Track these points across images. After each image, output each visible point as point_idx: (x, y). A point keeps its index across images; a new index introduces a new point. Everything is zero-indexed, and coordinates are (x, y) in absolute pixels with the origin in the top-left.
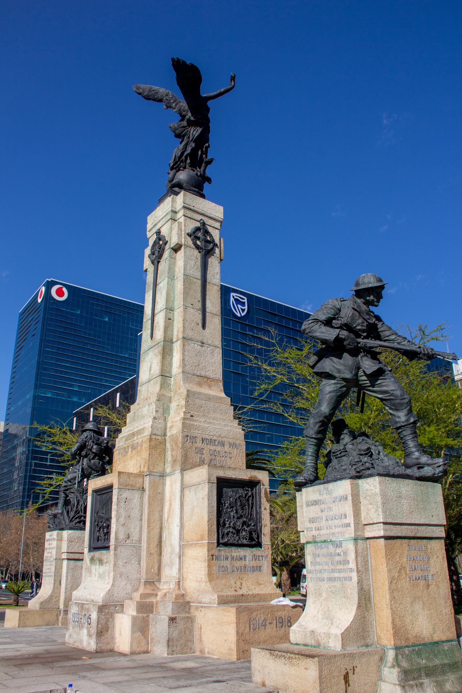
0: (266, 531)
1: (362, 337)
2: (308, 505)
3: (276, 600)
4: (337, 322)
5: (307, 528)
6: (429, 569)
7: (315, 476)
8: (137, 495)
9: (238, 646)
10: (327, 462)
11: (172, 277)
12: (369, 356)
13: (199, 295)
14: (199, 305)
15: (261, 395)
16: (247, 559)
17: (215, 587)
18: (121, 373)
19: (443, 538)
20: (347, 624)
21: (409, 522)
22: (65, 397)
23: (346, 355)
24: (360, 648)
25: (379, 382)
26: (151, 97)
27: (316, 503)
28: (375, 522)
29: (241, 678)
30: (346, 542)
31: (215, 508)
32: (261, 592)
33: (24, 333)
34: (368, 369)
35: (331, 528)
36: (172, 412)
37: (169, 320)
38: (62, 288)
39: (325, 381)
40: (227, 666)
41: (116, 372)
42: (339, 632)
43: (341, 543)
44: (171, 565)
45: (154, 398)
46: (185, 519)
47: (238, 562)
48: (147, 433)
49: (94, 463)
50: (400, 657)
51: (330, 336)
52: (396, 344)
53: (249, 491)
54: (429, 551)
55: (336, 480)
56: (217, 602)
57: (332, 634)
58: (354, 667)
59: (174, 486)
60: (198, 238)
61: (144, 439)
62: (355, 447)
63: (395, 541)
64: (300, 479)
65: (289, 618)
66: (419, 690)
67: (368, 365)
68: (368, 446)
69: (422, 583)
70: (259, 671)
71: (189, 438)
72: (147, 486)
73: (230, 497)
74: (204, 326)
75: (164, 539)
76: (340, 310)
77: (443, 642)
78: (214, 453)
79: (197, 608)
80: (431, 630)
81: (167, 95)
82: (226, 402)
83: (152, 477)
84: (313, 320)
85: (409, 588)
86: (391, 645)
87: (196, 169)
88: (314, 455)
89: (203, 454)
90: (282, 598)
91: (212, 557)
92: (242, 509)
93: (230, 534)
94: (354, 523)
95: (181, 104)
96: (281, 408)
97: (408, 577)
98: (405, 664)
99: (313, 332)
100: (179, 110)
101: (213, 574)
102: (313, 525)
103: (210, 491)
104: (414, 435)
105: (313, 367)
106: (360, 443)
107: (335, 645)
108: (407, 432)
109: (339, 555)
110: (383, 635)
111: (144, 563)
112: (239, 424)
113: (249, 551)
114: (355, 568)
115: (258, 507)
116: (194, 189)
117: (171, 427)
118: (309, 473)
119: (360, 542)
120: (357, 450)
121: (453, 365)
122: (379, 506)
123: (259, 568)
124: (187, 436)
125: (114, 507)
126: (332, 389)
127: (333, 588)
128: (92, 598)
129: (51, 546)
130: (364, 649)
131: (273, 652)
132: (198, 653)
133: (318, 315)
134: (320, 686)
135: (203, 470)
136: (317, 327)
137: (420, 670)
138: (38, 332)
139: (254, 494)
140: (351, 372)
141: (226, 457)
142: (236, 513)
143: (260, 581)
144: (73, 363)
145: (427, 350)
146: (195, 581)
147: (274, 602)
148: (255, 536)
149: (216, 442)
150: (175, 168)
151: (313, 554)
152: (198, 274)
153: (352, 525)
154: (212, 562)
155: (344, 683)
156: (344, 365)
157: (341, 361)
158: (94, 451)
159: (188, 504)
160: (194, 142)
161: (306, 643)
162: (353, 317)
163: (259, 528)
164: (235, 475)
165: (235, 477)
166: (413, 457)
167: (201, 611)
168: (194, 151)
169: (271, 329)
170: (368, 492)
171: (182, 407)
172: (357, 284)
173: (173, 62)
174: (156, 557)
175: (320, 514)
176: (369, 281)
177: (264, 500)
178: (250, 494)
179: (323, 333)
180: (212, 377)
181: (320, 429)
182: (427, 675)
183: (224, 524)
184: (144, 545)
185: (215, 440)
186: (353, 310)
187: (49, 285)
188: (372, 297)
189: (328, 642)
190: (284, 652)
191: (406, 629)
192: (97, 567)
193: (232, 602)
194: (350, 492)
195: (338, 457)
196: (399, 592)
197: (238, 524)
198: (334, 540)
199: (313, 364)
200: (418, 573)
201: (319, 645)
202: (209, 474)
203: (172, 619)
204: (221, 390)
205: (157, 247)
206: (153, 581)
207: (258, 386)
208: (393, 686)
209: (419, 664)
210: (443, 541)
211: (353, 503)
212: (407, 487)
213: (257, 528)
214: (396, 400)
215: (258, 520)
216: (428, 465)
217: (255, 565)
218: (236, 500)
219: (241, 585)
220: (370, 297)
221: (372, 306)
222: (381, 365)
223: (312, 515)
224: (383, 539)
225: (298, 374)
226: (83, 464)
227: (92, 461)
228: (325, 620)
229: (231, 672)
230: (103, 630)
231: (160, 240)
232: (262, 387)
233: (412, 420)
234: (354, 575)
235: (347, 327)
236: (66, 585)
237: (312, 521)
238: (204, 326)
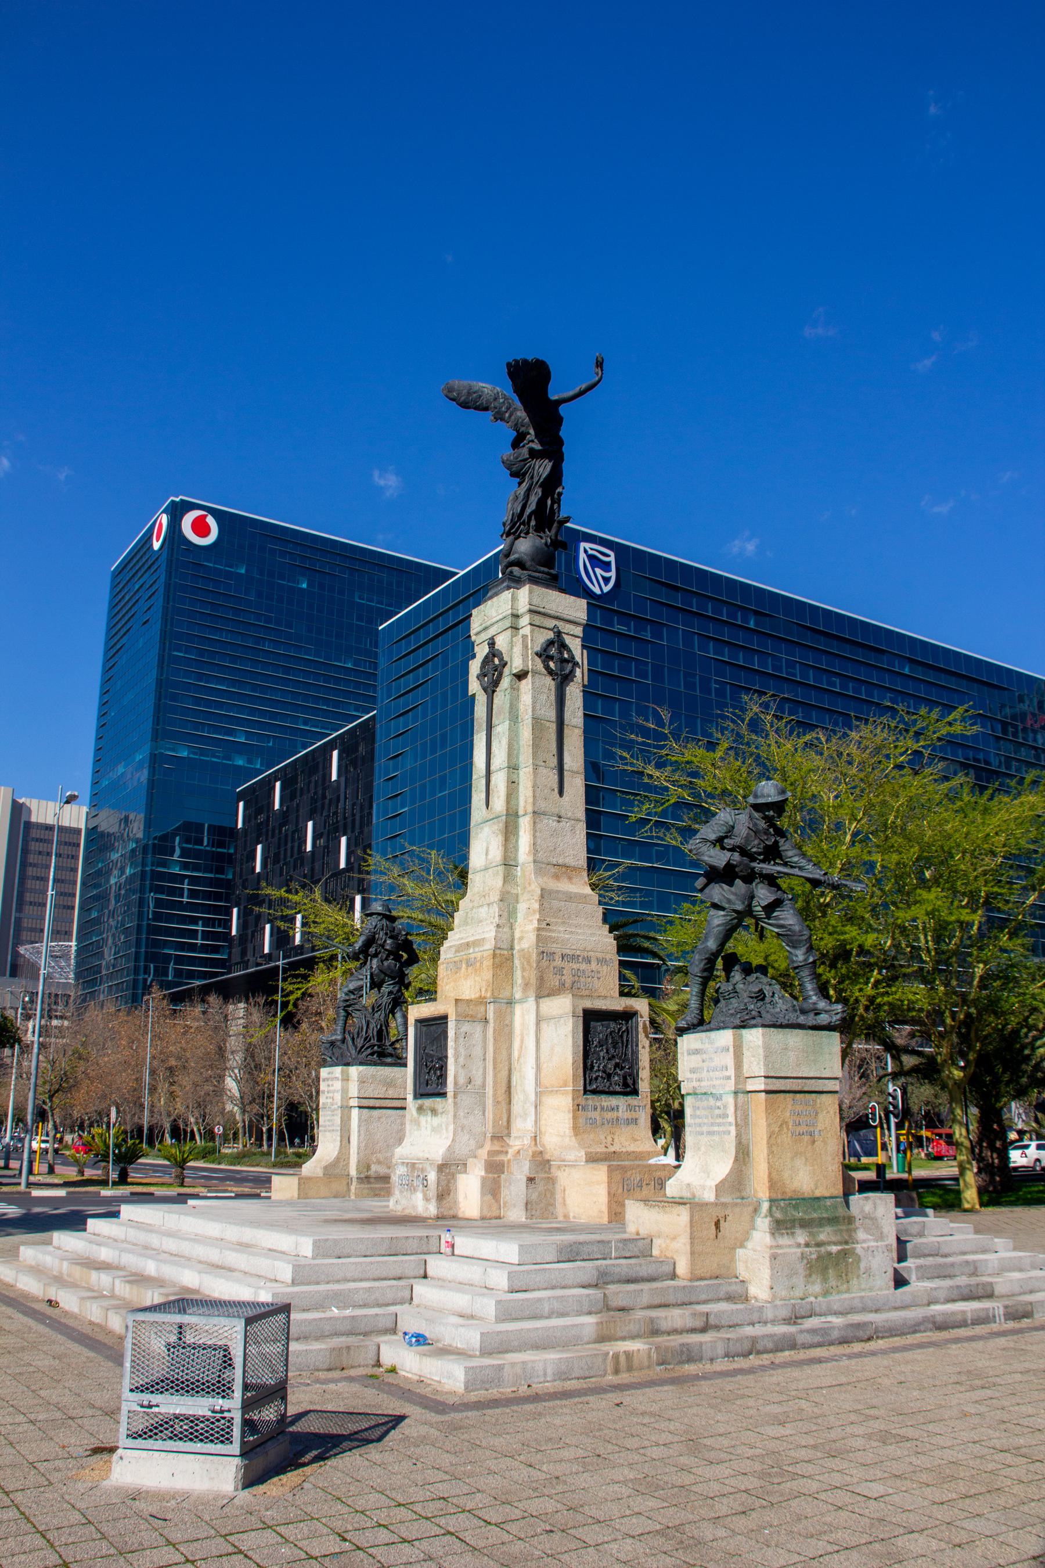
0: (644, 1075)
2: (689, 1054)
8: (478, 1028)
9: (610, 1207)
11: (514, 718)
12: (766, 882)
14: (554, 762)
18: (337, 704)
22: (218, 757)
23: (738, 882)
25: (775, 914)
26: (470, 403)
27: (697, 1052)
31: (581, 1048)
33: (124, 616)
35: (712, 1080)
36: (520, 916)
37: (512, 784)
38: (206, 516)
41: (326, 701)
44: (525, 1116)
45: (495, 897)
46: (542, 1059)
48: (489, 945)
49: (389, 966)
50: (774, 1209)
59: (526, 1017)
60: (551, 658)
61: (485, 954)
64: (683, 1024)
67: (764, 895)
68: (760, 986)
72: (491, 1016)
74: (561, 793)
75: (513, 1083)
76: (733, 827)
78: (577, 974)
79: (559, 1167)
80: (812, 1186)
81: (495, 399)
83: (497, 1005)
87: (544, 532)
90: (662, 1157)
91: (578, 1107)
92: (615, 1047)
95: (519, 414)
100: (516, 425)
102: (694, 1076)
103: (575, 1027)
107: (710, 1196)
110: (760, 1188)
111: (490, 1114)
114: (734, 1122)
116: (542, 569)
117: (521, 938)
119: (740, 1096)
123: (635, 1121)
125: (451, 1043)
128: (427, 1155)
129: (331, 1088)
130: (739, 1201)
132: (561, 1218)
136: (704, 849)
138: (156, 615)
142: (607, 1052)
144: (233, 683)
147: (652, 1161)
148: (630, 1081)
150: (514, 533)
152: (552, 714)
153: (733, 1078)
156: (735, 894)
157: (733, 889)
158: (388, 947)
159: (546, 1042)
160: (540, 486)
162: (747, 838)
168: (541, 503)
171: (534, 911)
173: (509, 369)
174: (504, 1105)
175: (701, 1064)
177: (641, 1036)
183: (592, 1067)
184: (489, 1091)
187: (177, 511)
192: (429, 1118)
200: (803, 1129)
201: (694, 1196)
203: (531, 1180)
205: (489, 668)
206: (501, 1135)
212: (795, 1039)
216: (826, 1011)
223: (693, 1065)
226: (371, 968)
227: (386, 963)
230: (444, 1193)
231: (494, 656)
236: (359, 1143)
237: (693, 1071)
238: (561, 793)
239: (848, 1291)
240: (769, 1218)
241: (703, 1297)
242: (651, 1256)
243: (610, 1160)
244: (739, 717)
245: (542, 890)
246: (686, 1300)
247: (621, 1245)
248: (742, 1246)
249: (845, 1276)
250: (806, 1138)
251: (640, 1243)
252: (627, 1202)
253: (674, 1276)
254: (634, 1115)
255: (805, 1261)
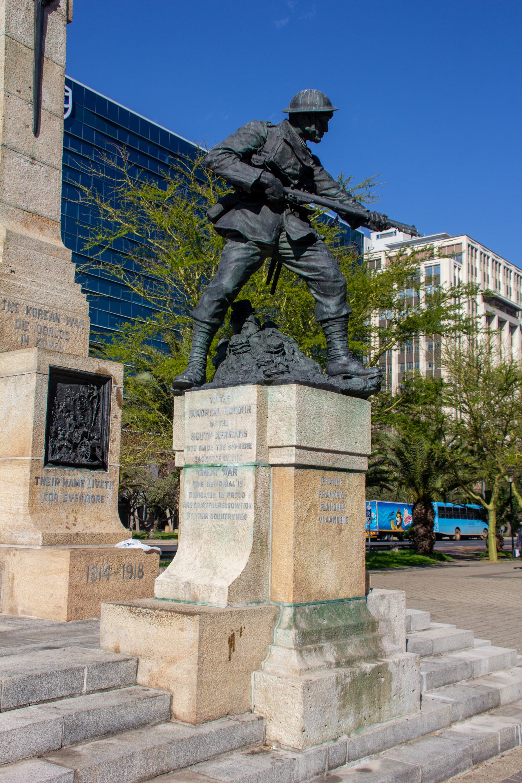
1: (292, 185)
2: (192, 415)
3: (123, 543)
4: (259, 158)
5: (188, 447)
6: (344, 510)
7: (202, 377)
10: (217, 358)
12: (298, 215)
13: (30, 77)
14: (30, 95)
15: (95, 250)
16: (86, 486)
17: (38, 523)
19: (365, 471)
20: (237, 574)
21: (327, 448)
23: (265, 209)
24: (250, 605)
25: (306, 254)
27: (204, 413)
28: (285, 444)
29: (81, 643)
30: (243, 468)
31: (45, 411)
32: (103, 531)
34: (294, 233)
35: (223, 448)
39: (231, 244)
40: (55, 629)
42: (226, 584)
43: (236, 470)
47: (73, 489)
50: (299, 616)
51: (248, 177)
52: (338, 202)
53: (94, 389)
54: (347, 487)
55: (235, 384)
56: (41, 543)
57: (215, 587)
58: (241, 628)
62: (262, 341)
63: (308, 471)
65: (141, 567)
66: (317, 655)
67: (296, 229)
68: (282, 341)
69: (334, 526)
70: (112, 634)
71: (7, 304)
73: (67, 397)
74: (36, 132)
76: (265, 141)
77: (350, 599)
78: (43, 331)
82: (65, 256)
84: (224, 149)
85: (318, 532)
86: (288, 602)
88: (204, 347)
89: (28, 330)
90: (131, 541)
91: (36, 480)
92: (83, 414)
93: (64, 449)
94: (257, 444)
96: (123, 273)
97: (318, 519)
98: (303, 625)
99: (222, 167)
101: (37, 504)
102: (197, 443)
104: (343, 333)
105: (215, 220)
106: (269, 336)
107: (219, 601)
108: (335, 328)
109: (231, 484)
110: (281, 588)
112: (83, 291)
113: (88, 474)
115: (106, 413)
118: (195, 371)
119: (262, 469)
120: (264, 345)
121: (365, 238)
122: (293, 424)
123: (101, 499)
124: (5, 301)
126: (240, 256)
127: (218, 528)
130: (255, 607)
131: (134, 608)
133: (232, 142)
134: (199, 650)
135: (29, 354)
137: (320, 632)
139: (101, 394)
140: (270, 235)
141: (61, 338)
142: (75, 419)
143: (101, 516)
145: (379, 217)
146: (7, 513)
148: (98, 453)
149: (48, 314)
151: (194, 482)
152: (30, 39)
153: (254, 447)
154: (35, 486)
155: (228, 647)
156: (262, 224)
157: (258, 217)
161: (176, 598)
163: (105, 442)
164: (76, 365)
165: (76, 368)
166: (340, 362)
167: (14, 555)
169: (122, 150)
170: (279, 404)
172: (295, 104)
175: (209, 429)
176: (312, 101)
177: (114, 404)
178: (95, 394)
179: (237, 171)
180: (45, 214)
181: (217, 311)
182: (328, 638)
183: (57, 435)
185: (46, 312)
186: (284, 143)
188: (313, 128)
189: (209, 597)
190: (150, 609)
191: (309, 583)
193: (62, 544)
194: (256, 403)
195: (238, 353)
196: (305, 536)
197: (76, 435)
198: (225, 465)
199: (216, 215)
201: (195, 600)
202: (39, 361)
204: (58, 237)
207: (92, 235)
208: (288, 650)
209: (320, 625)
210: (364, 476)
211: (258, 417)
212: (330, 402)
213: (102, 442)
214: (327, 281)
215: (105, 431)
216: (358, 375)
217: (96, 494)
218: (75, 400)
219: (75, 521)
220: (310, 126)
221: (311, 141)
222: (312, 229)
224: (293, 468)
225: (154, 225)
228: (205, 569)
229: (64, 636)
232: (99, 237)
233: (344, 312)
234: (251, 513)
235: (272, 167)
237: (196, 437)
238: (36, 132)
239: (380, 720)
240: (294, 631)
241: (214, 749)
242: (136, 684)
243: (72, 544)
244: (188, 163)
245: (8, 232)
246: (191, 758)
247: (96, 673)
248: (258, 668)
249: (376, 704)
250: (334, 526)
251: (122, 667)
252: (103, 606)
253: (169, 716)
254: (100, 492)
255: (340, 688)
